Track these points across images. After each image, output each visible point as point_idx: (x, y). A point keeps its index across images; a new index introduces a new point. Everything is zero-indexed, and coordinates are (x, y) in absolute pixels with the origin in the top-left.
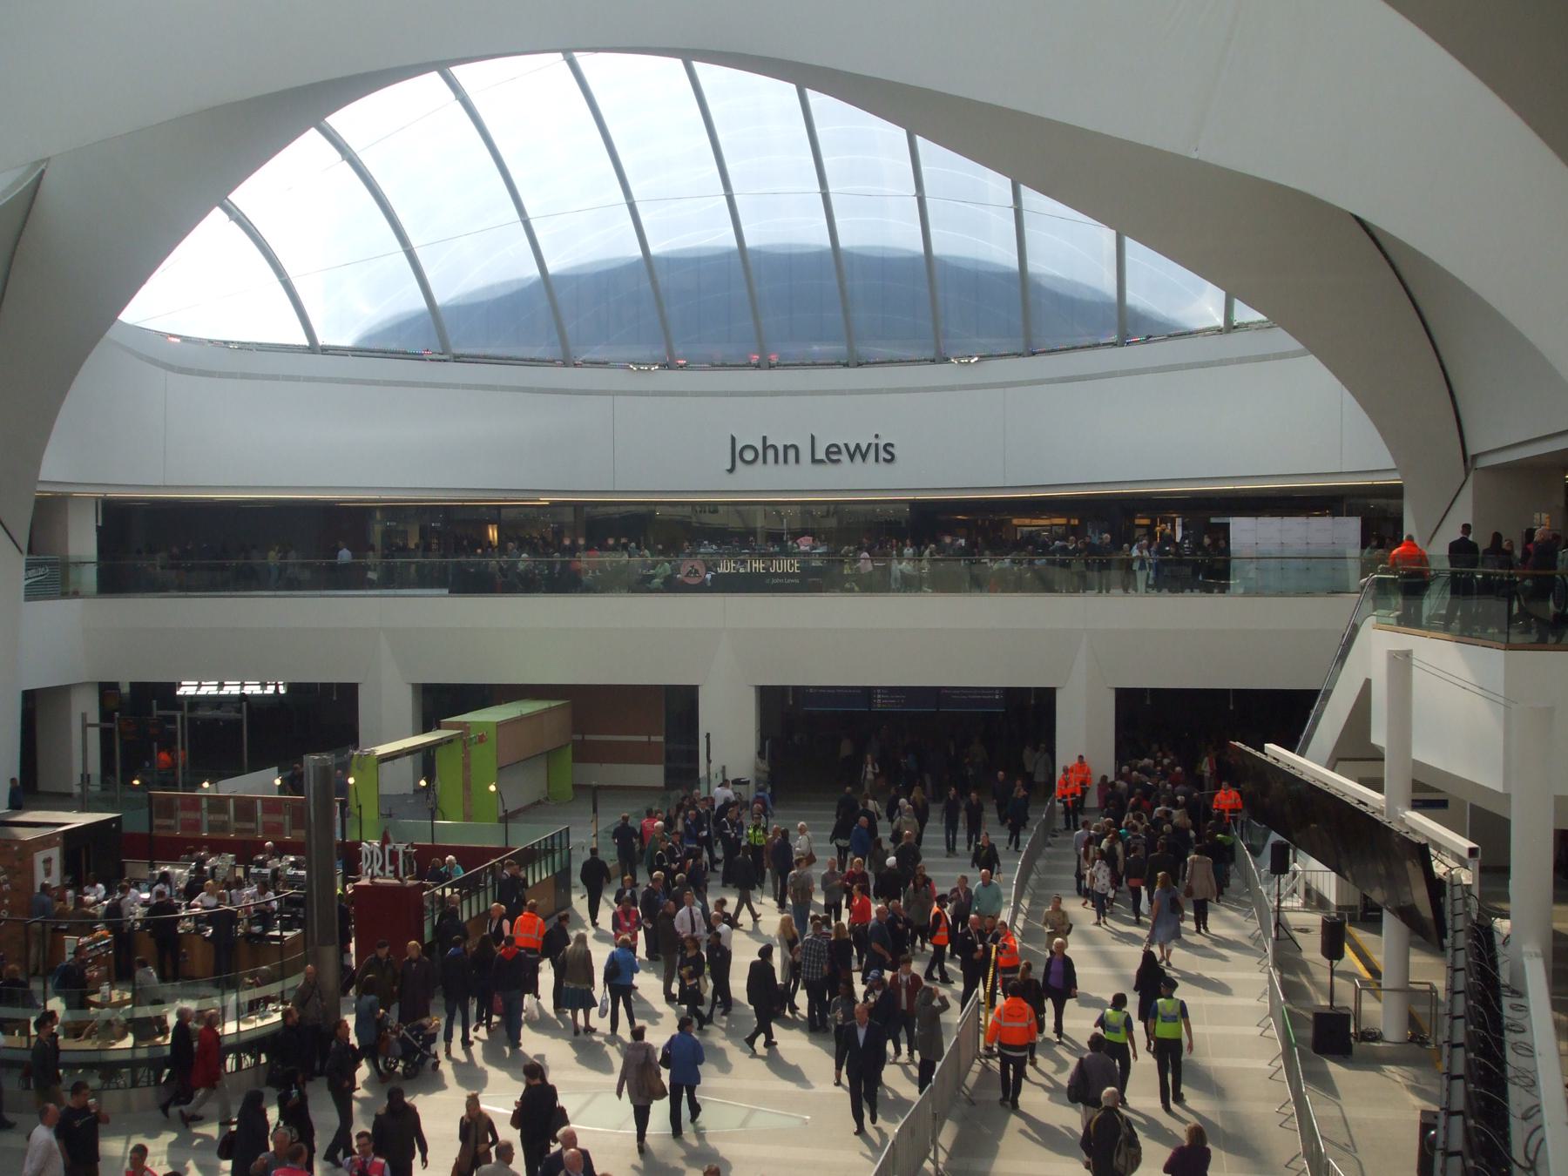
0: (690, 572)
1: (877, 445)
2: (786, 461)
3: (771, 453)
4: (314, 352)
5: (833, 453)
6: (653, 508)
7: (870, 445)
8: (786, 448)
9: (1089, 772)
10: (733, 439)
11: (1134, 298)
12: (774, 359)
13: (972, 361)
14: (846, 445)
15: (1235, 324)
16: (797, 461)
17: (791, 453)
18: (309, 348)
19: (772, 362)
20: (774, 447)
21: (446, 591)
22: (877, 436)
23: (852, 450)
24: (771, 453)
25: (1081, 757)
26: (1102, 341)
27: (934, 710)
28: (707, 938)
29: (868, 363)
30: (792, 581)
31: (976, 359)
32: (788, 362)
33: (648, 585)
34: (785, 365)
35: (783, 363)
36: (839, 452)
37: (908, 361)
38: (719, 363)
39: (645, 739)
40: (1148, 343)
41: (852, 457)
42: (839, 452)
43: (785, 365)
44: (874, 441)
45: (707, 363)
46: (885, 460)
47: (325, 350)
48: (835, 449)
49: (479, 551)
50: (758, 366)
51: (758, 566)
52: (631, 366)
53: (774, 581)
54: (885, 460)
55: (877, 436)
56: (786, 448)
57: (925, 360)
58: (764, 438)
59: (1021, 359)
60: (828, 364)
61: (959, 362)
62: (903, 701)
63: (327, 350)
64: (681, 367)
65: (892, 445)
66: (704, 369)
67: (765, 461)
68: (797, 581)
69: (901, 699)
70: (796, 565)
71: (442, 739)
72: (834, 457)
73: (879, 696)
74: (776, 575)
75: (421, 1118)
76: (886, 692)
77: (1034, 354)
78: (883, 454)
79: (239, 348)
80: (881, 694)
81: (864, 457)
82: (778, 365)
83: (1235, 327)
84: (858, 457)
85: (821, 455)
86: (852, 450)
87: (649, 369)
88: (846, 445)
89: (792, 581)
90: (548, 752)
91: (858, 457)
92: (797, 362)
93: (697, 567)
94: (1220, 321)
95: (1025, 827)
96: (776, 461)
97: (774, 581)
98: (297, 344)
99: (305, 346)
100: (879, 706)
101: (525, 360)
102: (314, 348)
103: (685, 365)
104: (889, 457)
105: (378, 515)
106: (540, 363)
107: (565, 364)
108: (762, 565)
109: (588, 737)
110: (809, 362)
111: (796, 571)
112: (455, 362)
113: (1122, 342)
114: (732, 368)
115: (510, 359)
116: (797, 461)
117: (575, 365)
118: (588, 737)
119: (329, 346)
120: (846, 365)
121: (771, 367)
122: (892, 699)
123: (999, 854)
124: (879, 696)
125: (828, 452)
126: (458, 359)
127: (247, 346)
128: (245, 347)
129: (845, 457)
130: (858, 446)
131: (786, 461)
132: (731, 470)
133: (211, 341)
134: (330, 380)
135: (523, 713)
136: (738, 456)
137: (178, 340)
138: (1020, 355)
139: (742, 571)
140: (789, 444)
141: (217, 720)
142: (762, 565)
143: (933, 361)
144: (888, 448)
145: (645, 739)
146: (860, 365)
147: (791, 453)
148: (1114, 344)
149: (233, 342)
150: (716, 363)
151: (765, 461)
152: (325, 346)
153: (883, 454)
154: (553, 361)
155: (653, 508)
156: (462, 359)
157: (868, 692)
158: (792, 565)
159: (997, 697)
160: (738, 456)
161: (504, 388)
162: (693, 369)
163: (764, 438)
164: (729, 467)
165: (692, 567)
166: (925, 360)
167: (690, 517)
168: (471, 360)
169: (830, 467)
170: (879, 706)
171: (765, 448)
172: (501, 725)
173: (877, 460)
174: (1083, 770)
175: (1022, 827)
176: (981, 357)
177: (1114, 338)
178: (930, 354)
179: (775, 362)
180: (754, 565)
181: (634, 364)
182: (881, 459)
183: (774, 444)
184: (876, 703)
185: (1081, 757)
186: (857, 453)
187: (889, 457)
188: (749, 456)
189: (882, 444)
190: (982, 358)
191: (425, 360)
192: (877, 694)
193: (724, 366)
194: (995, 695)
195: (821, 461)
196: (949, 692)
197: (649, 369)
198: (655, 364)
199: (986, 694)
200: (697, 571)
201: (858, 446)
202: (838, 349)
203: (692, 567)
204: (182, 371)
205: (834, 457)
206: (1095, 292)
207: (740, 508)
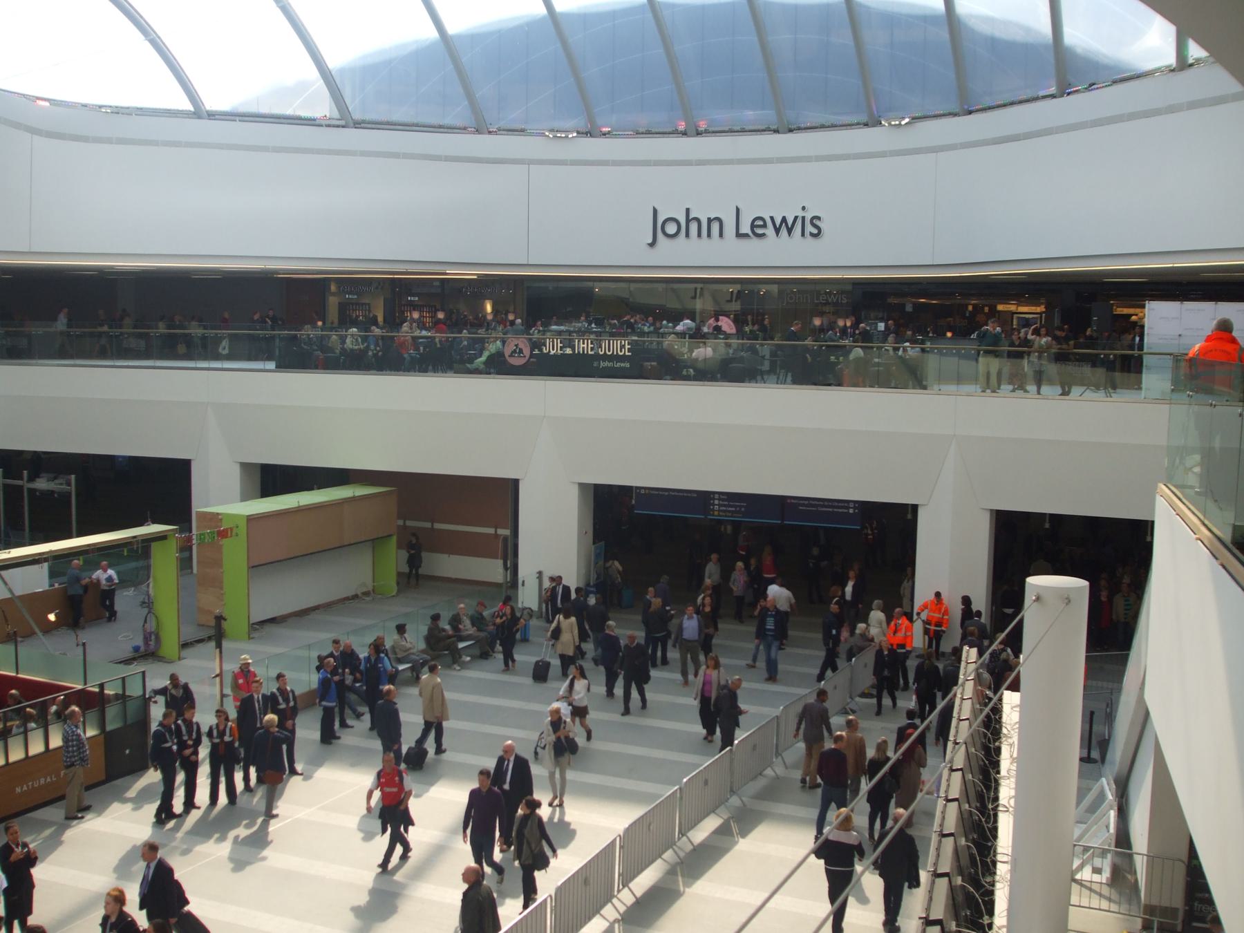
0: (515, 351)
1: (803, 218)
2: (709, 235)
3: (694, 227)
4: (200, 117)
5: (758, 225)
6: (590, 284)
7: (796, 218)
8: (710, 221)
9: (946, 612)
10: (655, 211)
11: (1074, 36)
12: (703, 126)
13: (903, 123)
14: (772, 218)
15: (1191, 61)
16: (721, 235)
17: (715, 227)
18: (194, 113)
19: (700, 129)
20: (698, 220)
21: (271, 365)
22: (804, 208)
23: (778, 223)
24: (694, 227)
25: (938, 595)
26: (1041, 93)
27: (779, 522)
28: (907, 611)
29: (799, 129)
30: (623, 365)
31: (907, 120)
32: (716, 129)
33: (468, 365)
34: (714, 132)
35: (711, 129)
36: (765, 226)
37: (841, 126)
38: (644, 130)
39: (491, 531)
40: (1090, 90)
41: (777, 231)
42: (765, 226)
43: (714, 132)
44: (800, 214)
45: (632, 131)
46: (812, 235)
47: (212, 115)
48: (761, 223)
49: (320, 323)
50: (684, 134)
51: (584, 346)
52: (547, 134)
53: (602, 364)
54: (812, 235)
55: (804, 208)
56: (710, 221)
57: (858, 124)
58: (688, 210)
59: (957, 118)
60: (758, 131)
61: (890, 124)
62: (743, 509)
63: (214, 115)
64: (604, 134)
65: (819, 218)
66: (628, 136)
67: (687, 235)
68: (628, 365)
69: (741, 507)
70: (627, 347)
71: (135, 537)
72: (760, 231)
73: (716, 502)
74: (605, 357)
75: (384, 853)
76: (725, 497)
77: (970, 113)
78: (810, 229)
79: (112, 112)
80: (719, 499)
81: (790, 231)
82: (706, 132)
83: (1191, 65)
84: (784, 231)
85: (745, 229)
86: (778, 223)
87: (567, 137)
88: (772, 218)
89: (623, 365)
90: (373, 540)
91: (784, 231)
92: (727, 129)
93: (521, 346)
94: (1171, 59)
95: (739, 727)
96: (699, 235)
97: (602, 364)
98: (180, 109)
99: (190, 111)
100: (716, 513)
101: (434, 127)
102: (199, 113)
103: (609, 133)
104: (815, 231)
105: (333, 288)
106: (449, 131)
107: (478, 131)
108: (590, 346)
109: (438, 526)
110: (738, 128)
111: (627, 354)
112: (356, 128)
113: (1064, 90)
114: (658, 135)
115: (417, 125)
116: (721, 235)
117: (490, 132)
118: (438, 526)
119: (216, 111)
120: (776, 131)
121: (699, 134)
122: (732, 506)
123: (908, 668)
124: (716, 502)
125: (753, 226)
126: (358, 124)
127: (124, 111)
128: (118, 111)
129: (770, 231)
130: (784, 220)
131: (709, 235)
132: (652, 245)
133: (85, 106)
134: (220, 146)
135: (301, 504)
136: (660, 228)
137: (47, 104)
138: (955, 115)
139: (569, 351)
140: (712, 217)
141: (53, 492)
142: (559, 345)
143: (866, 125)
144: (814, 221)
145: (491, 531)
146: (791, 131)
147: (715, 227)
148: (1053, 96)
149: (106, 106)
150: (641, 130)
151: (687, 235)
152: (212, 111)
153: (810, 229)
154: (465, 129)
155: (590, 284)
156: (362, 125)
157: (704, 498)
158: (623, 347)
159: (851, 511)
160: (660, 228)
161: (364, 154)
162: (616, 136)
163: (688, 210)
164: (650, 241)
165: (516, 346)
166: (858, 124)
167: (628, 299)
168: (373, 126)
169: (755, 241)
170: (716, 513)
171: (688, 221)
172: (251, 519)
173: (803, 235)
174: (940, 610)
175: (737, 728)
176: (913, 119)
177: (1053, 90)
178: (864, 119)
179: (703, 129)
180: (582, 346)
181: (551, 131)
182: (807, 233)
183: (699, 217)
184: (713, 510)
185: (938, 595)
186: (784, 226)
187: (815, 231)
188: (671, 229)
189: (808, 216)
190: (915, 119)
191: (322, 126)
192: (714, 499)
193: (649, 133)
194: (848, 508)
195: (746, 235)
196: (795, 501)
197: (567, 137)
198: (572, 132)
199: (826, 507)
200: (521, 352)
201: (784, 220)
202: (768, 116)
203: (516, 346)
204: (50, 135)
205: (760, 231)
206: (1028, 30)
207: (676, 286)
